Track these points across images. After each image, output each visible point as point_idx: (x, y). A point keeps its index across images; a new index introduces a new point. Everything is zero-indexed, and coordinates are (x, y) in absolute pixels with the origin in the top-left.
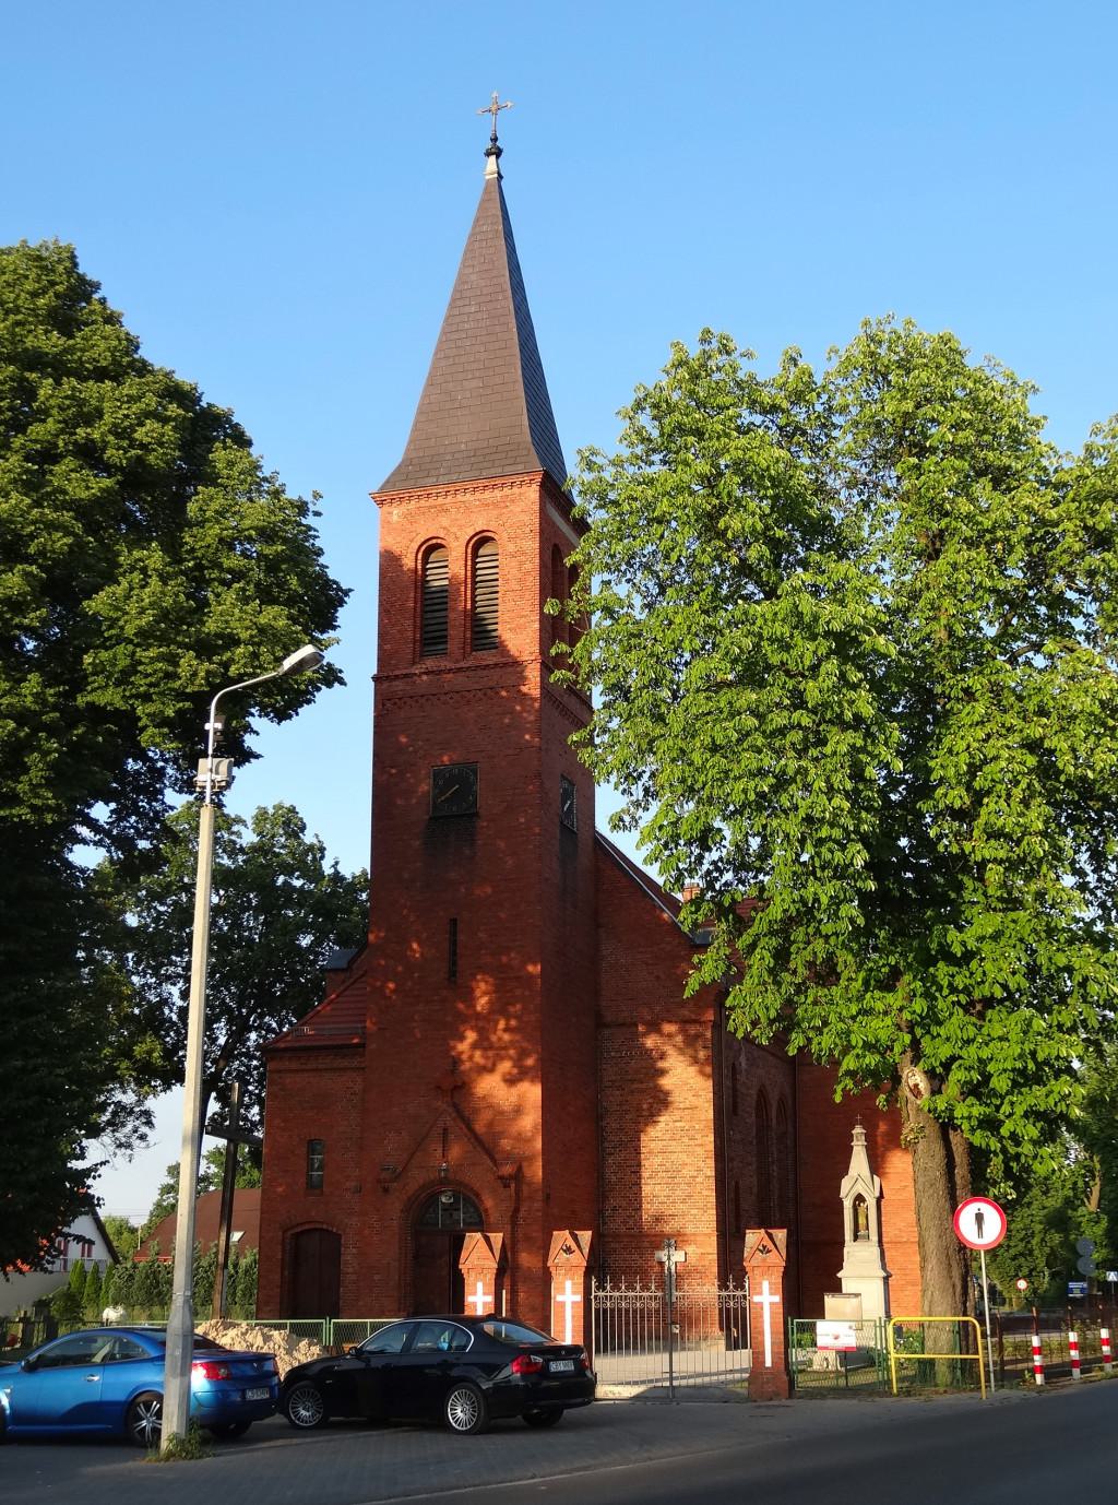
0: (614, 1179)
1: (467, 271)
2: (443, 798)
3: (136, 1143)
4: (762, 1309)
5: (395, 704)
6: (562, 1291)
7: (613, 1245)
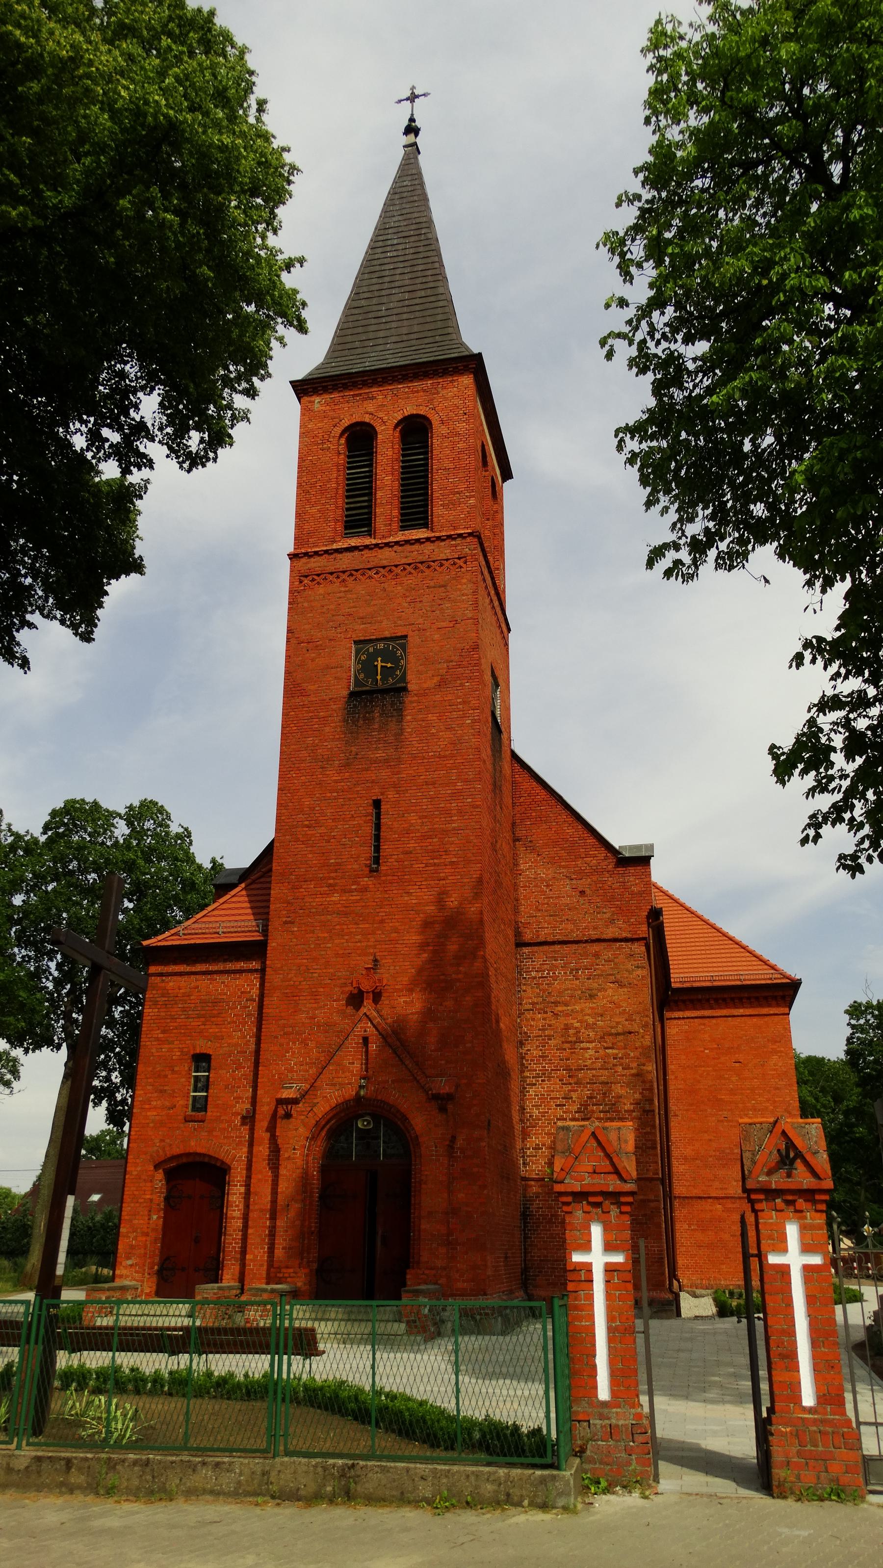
0: (536, 1112)
1: (386, 220)
5: (313, 580)
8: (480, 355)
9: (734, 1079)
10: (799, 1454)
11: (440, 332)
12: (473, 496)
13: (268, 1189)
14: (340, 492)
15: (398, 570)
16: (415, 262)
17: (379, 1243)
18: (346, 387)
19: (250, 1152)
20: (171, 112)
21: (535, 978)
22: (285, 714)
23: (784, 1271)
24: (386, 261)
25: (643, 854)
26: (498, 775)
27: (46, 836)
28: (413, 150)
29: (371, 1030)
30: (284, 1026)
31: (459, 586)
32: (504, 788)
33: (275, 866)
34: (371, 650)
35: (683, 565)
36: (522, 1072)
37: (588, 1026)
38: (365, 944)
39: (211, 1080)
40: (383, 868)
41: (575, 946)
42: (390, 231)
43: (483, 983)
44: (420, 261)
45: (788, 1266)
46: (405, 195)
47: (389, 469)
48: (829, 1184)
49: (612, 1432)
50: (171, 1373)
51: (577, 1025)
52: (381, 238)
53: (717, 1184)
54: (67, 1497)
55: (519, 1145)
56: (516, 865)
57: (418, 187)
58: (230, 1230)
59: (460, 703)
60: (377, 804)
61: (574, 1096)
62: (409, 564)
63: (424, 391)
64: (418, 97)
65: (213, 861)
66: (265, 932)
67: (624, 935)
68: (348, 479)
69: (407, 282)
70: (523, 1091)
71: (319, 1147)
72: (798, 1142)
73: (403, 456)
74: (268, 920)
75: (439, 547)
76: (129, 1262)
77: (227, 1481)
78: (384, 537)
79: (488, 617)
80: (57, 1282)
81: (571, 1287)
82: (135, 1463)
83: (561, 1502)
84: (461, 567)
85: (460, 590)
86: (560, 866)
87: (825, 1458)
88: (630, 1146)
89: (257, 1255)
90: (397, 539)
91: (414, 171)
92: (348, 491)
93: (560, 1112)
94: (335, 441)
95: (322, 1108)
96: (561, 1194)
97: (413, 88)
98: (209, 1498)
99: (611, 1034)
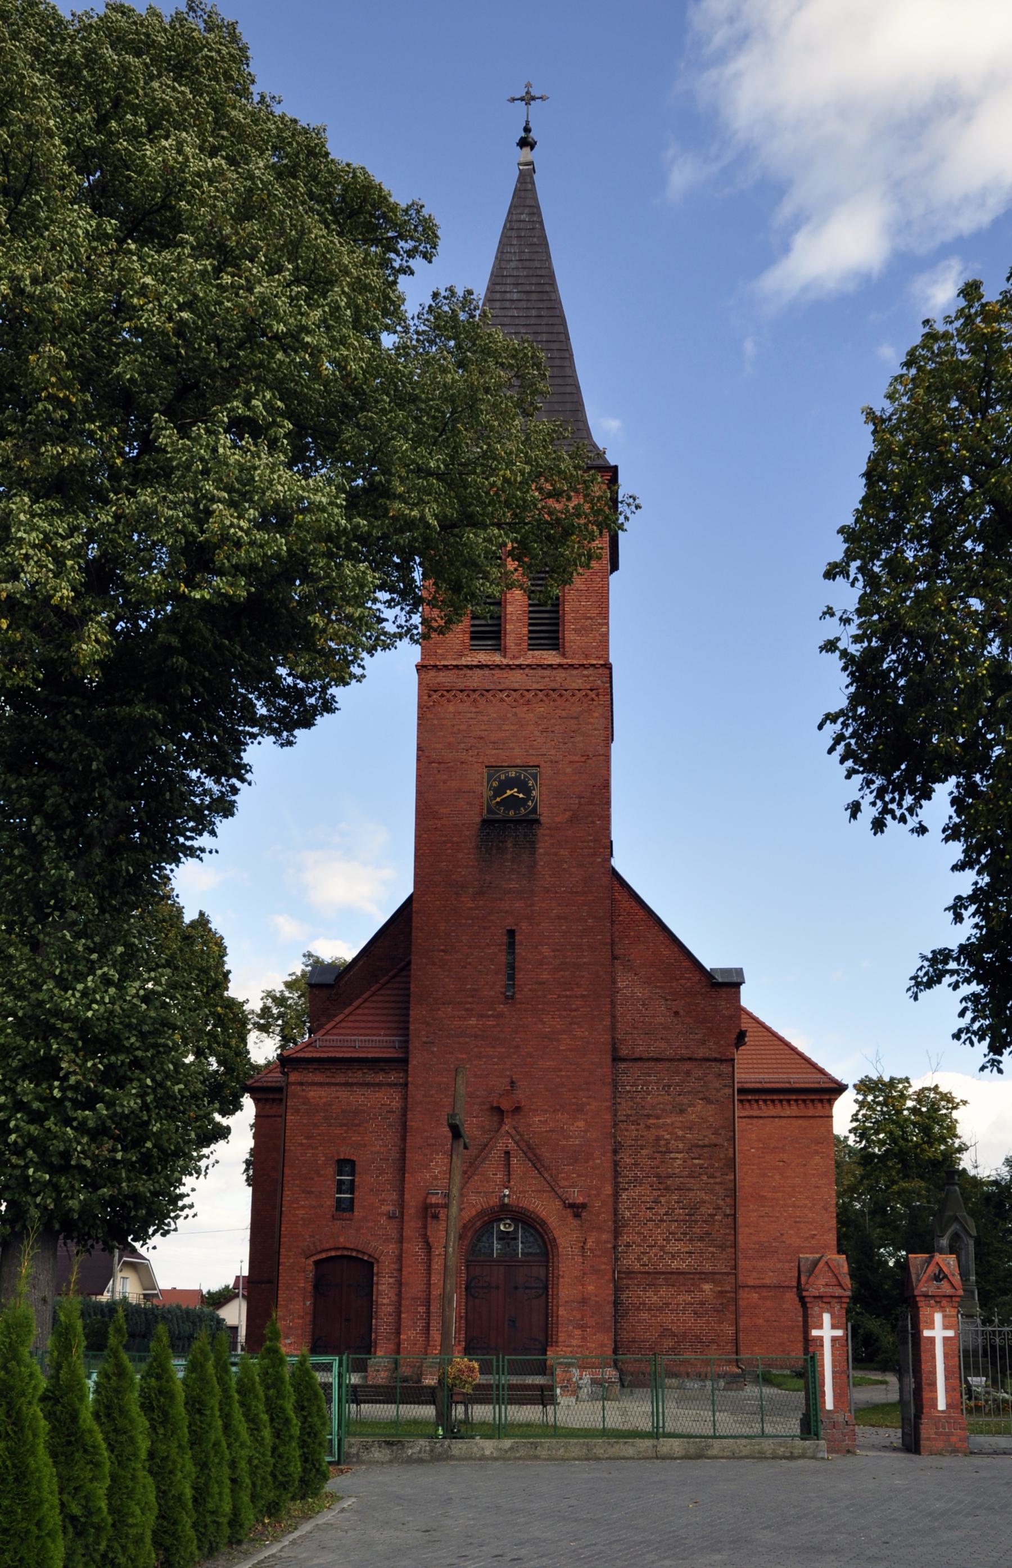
0: (627, 1214)
2: (498, 799)
5: (442, 696)
6: (931, 1326)
7: (625, 1282)
8: (616, 468)
9: (777, 1177)
10: (936, 1433)
16: (539, 329)
21: (629, 1092)
23: (932, 1340)
29: (512, 1145)
31: (591, 720)
37: (678, 1138)
38: (501, 1067)
39: (356, 1184)
41: (667, 1065)
45: (934, 1338)
48: (961, 1292)
51: (668, 1137)
53: (754, 1275)
56: (614, 983)
59: (591, 841)
61: (663, 1200)
62: (541, 690)
64: (533, 98)
67: (715, 1055)
72: (945, 1269)
74: (407, 1035)
75: (571, 676)
78: (514, 657)
82: (576, 1444)
84: (593, 700)
85: (591, 724)
86: (656, 987)
87: (949, 1434)
93: (649, 1214)
99: (698, 1146)
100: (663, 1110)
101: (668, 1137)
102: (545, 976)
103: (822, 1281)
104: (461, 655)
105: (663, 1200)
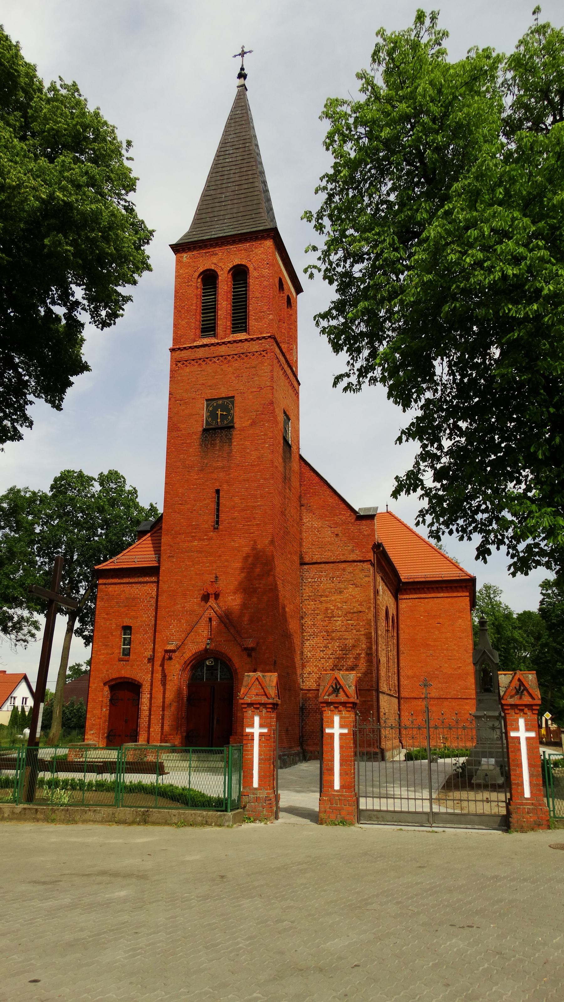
0: (309, 654)
1: (226, 137)
3: (29, 638)
4: (519, 743)
10: (330, 808)
11: (255, 212)
12: (272, 314)
13: (161, 696)
14: (198, 311)
15: (230, 358)
16: (242, 166)
17: (215, 723)
18: (201, 248)
19: (152, 677)
20: (65, 199)
22: (168, 442)
24: (226, 165)
25: (371, 513)
26: (287, 471)
27: (52, 493)
28: (243, 87)
29: (213, 614)
30: (169, 612)
32: (293, 478)
33: (164, 526)
34: (215, 404)
35: (353, 385)
36: (303, 633)
37: (338, 609)
40: (220, 527)
41: (332, 565)
42: (228, 144)
43: (273, 590)
44: (245, 165)
46: (237, 120)
47: (225, 298)
49: (257, 799)
50: (96, 781)
51: (333, 608)
52: (222, 149)
54: (36, 823)
55: (299, 672)
56: (301, 519)
57: (245, 115)
58: (142, 716)
60: (218, 491)
61: (330, 646)
63: (245, 250)
64: (245, 53)
65: (151, 505)
66: (159, 561)
67: (359, 558)
68: (203, 303)
69: (237, 179)
70: (303, 643)
71: (187, 675)
73: (234, 288)
74: (160, 554)
76: (92, 732)
77: (98, 817)
78: (222, 338)
79: (283, 381)
80: (37, 740)
81: (244, 742)
82: (62, 810)
83: (227, 824)
85: (264, 370)
87: (340, 810)
88: (274, 683)
89: (156, 729)
90: (229, 340)
91: (243, 104)
92: (203, 310)
93: (322, 654)
94: (195, 280)
95: (188, 655)
96: (242, 704)
97: (243, 47)
98: (91, 823)
99: (350, 613)
100: (330, 592)
101: (333, 608)
102: (236, 514)
103: (254, 691)
104: (195, 341)
105: (330, 646)
